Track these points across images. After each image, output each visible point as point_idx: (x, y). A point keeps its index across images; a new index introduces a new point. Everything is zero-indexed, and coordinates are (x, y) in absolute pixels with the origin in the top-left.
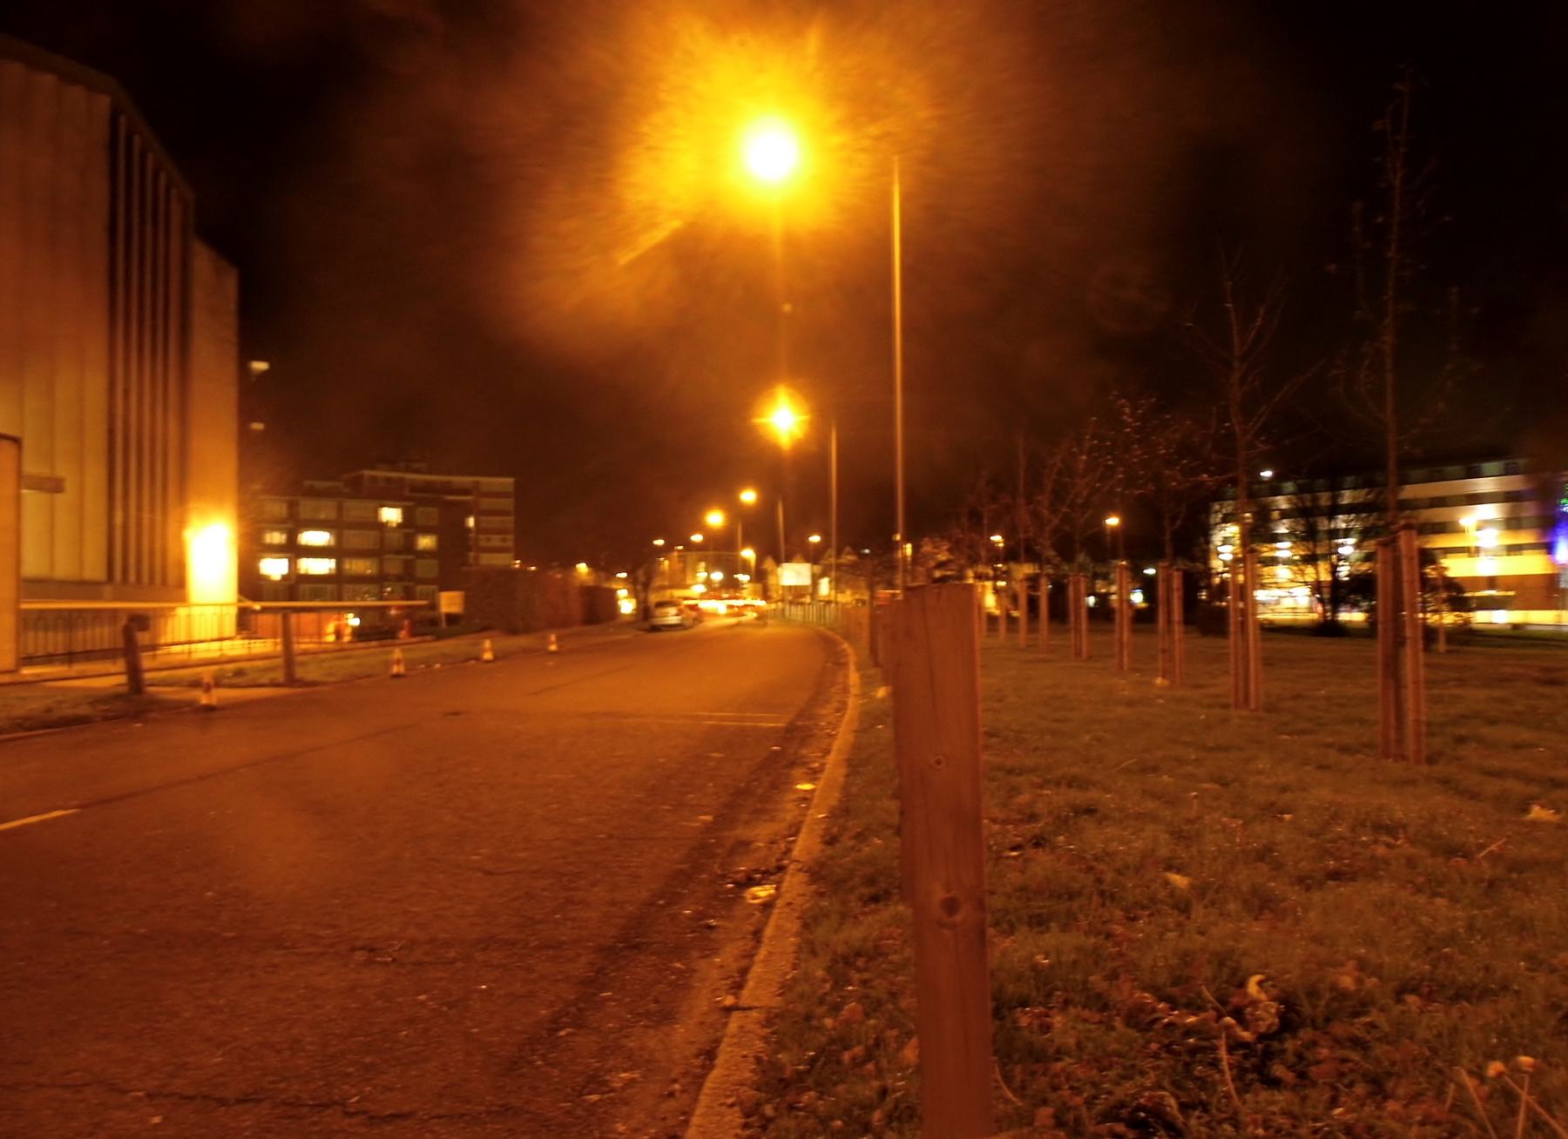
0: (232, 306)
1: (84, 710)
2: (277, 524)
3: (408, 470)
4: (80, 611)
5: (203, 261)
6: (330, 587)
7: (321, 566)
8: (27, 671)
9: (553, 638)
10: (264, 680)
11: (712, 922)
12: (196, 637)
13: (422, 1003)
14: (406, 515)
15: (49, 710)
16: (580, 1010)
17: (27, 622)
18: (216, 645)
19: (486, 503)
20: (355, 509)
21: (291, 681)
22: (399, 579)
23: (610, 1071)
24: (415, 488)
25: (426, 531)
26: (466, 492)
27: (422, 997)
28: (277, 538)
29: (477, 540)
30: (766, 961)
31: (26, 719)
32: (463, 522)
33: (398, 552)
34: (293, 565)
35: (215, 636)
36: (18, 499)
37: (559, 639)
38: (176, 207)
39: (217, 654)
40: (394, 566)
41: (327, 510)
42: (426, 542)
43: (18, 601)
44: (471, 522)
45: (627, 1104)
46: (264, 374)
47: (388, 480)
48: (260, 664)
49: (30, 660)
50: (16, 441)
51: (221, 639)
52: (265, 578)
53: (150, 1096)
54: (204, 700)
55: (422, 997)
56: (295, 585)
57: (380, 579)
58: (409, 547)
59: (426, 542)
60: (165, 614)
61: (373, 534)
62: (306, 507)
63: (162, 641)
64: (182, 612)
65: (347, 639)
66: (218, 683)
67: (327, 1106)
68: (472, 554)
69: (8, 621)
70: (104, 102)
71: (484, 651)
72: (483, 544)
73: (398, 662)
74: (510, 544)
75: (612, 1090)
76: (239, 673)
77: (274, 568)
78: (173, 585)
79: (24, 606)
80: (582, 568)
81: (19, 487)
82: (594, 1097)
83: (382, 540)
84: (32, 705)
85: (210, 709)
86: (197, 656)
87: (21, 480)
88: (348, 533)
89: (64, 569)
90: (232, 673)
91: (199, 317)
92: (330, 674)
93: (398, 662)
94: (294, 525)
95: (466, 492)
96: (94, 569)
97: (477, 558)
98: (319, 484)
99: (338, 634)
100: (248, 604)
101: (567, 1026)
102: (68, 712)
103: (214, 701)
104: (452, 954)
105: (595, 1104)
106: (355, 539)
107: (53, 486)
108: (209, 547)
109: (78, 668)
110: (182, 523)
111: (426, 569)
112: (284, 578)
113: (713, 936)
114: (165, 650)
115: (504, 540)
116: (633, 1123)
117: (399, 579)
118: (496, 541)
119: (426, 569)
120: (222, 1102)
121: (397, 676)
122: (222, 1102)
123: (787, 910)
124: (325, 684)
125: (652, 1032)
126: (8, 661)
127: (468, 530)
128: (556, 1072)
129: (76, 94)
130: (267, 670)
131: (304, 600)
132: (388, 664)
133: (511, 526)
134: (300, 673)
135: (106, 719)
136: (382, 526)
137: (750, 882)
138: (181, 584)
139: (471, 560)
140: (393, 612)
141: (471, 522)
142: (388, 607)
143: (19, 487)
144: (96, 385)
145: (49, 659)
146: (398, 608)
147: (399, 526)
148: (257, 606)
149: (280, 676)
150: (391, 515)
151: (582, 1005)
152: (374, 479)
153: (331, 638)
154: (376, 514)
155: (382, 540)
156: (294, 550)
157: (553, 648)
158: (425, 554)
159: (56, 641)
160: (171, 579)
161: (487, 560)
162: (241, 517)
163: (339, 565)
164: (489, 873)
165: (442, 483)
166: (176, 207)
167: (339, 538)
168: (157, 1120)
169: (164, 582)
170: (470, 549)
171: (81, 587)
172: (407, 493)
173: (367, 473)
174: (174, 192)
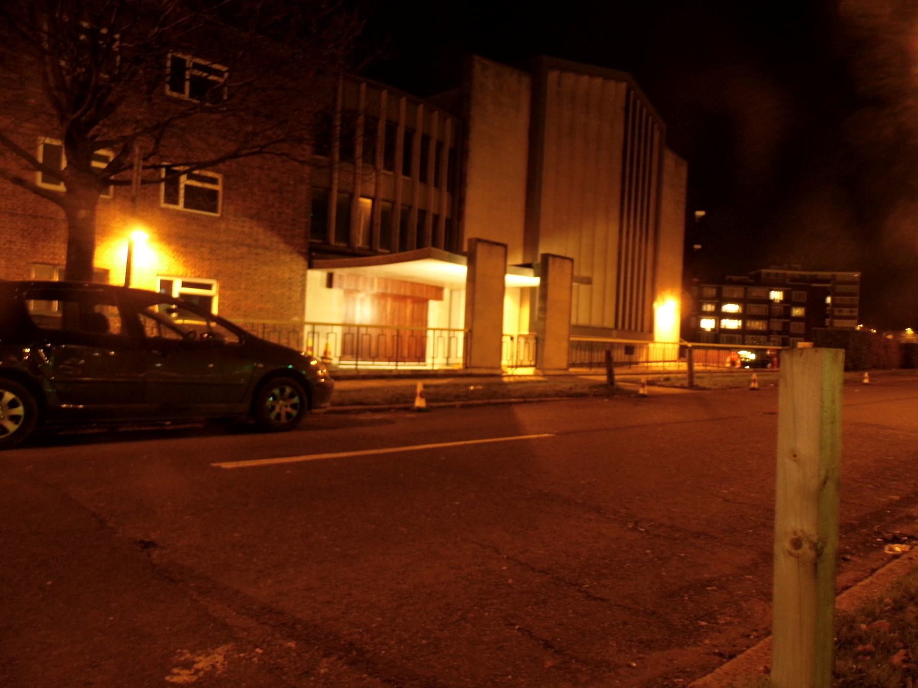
0: (684, 183)
1: (586, 390)
2: (710, 300)
3: (790, 268)
4: (597, 342)
5: (670, 159)
6: (738, 336)
7: (732, 324)
8: (572, 370)
9: (866, 375)
10: (678, 385)
11: (849, 557)
12: (667, 359)
13: (647, 554)
14: (785, 296)
15: (571, 389)
16: (728, 580)
17: (576, 346)
18: (660, 364)
19: (840, 288)
20: (756, 292)
21: (691, 386)
22: (779, 333)
23: (722, 614)
24: (793, 279)
25: (798, 305)
26: (827, 281)
27: (648, 551)
28: (709, 308)
29: (832, 311)
30: (864, 586)
31: (561, 391)
32: (824, 300)
33: (779, 317)
34: (718, 323)
35: (661, 359)
36: (571, 288)
37: (869, 375)
38: (657, 134)
39: (661, 369)
40: (777, 325)
41: (739, 292)
42: (797, 312)
43: (569, 337)
44: (829, 300)
45: (720, 632)
46: (703, 217)
47: (777, 275)
48: (680, 376)
49: (573, 365)
50: (572, 260)
51: (664, 361)
52: (703, 330)
53: (508, 558)
54: (641, 391)
55: (648, 551)
56: (719, 334)
57: (768, 333)
58: (787, 314)
59: (797, 312)
60: (641, 346)
61: (765, 306)
62: (727, 290)
63: (641, 360)
64: (651, 345)
65: (738, 366)
66: (650, 383)
67: (573, 585)
68: (828, 320)
69: (565, 345)
70: (623, 86)
71: (864, 378)
72: (836, 313)
73: (755, 381)
74: (856, 314)
75: (717, 624)
76: (667, 379)
77: (707, 324)
78: (646, 330)
79: (572, 339)
80: (909, 331)
81: (572, 282)
82: (704, 623)
83: (770, 309)
84: (566, 385)
85: (643, 396)
86: (650, 370)
87: (573, 279)
88: (749, 305)
89: (596, 322)
90: (666, 379)
91: (666, 191)
92: (715, 385)
93: (755, 381)
94: (720, 300)
95: (827, 281)
96: (609, 323)
97: (831, 323)
98: (735, 278)
99: (733, 363)
100: (685, 343)
101: (715, 585)
102: (579, 390)
103: (646, 392)
104: (677, 535)
105: (702, 626)
106: (754, 309)
107: (588, 281)
108: (667, 312)
109: (594, 370)
110: (653, 299)
111: (799, 328)
112: (713, 330)
113: (844, 565)
114: (642, 365)
115: (851, 312)
116: (715, 642)
117: (779, 333)
118: (846, 312)
119: (795, 327)
120: (533, 569)
121: (754, 389)
122: (533, 569)
123: (907, 562)
124: (710, 389)
125: (762, 603)
126: (564, 365)
127: (827, 305)
128: (692, 605)
129: (612, 85)
130: (678, 379)
131: (723, 343)
132: (750, 382)
133: (857, 303)
134: (697, 382)
135: (594, 396)
136: (771, 302)
137: (896, 540)
138: (651, 330)
139: (827, 324)
140: (768, 353)
141: (829, 300)
142: (765, 350)
143: (572, 282)
144: (614, 229)
145: (581, 365)
146: (772, 350)
147: (781, 302)
148: (690, 345)
149: (686, 383)
150: (776, 295)
151: (731, 578)
152: (768, 274)
153: (728, 365)
154: (768, 294)
155: (770, 309)
156: (719, 315)
157: (866, 381)
158: (797, 319)
159: (584, 356)
160: (646, 328)
161: (838, 323)
162: (683, 298)
163: (744, 324)
164: (727, 501)
165: (811, 276)
166: (657, 134)
167: (744, 308)
168: (504, 568)
169: (642, 330)
170: (827, 316)
171: (602, 331)
172: (788, 282)
173: (764, 271)
174: (656, 126)
